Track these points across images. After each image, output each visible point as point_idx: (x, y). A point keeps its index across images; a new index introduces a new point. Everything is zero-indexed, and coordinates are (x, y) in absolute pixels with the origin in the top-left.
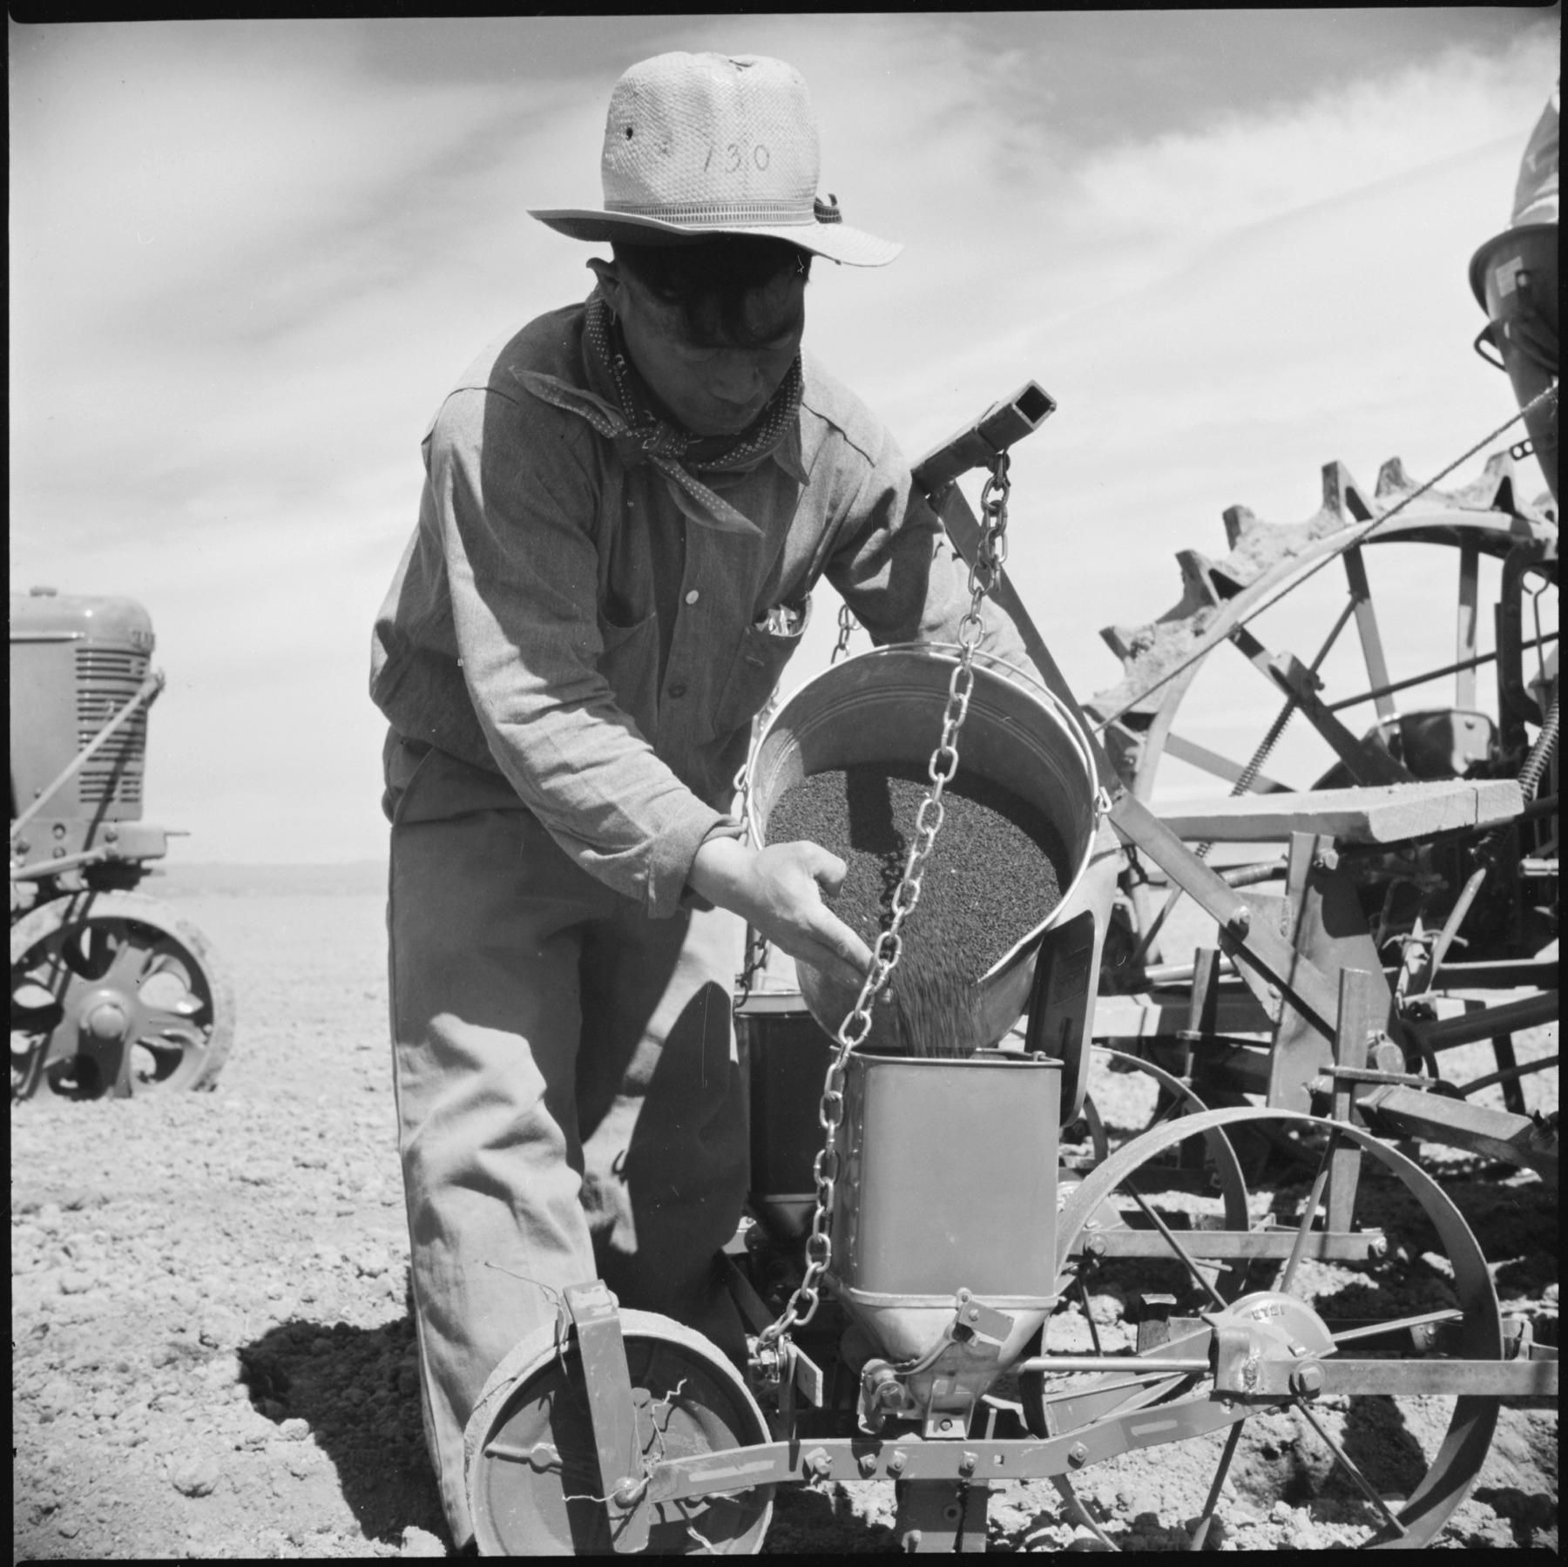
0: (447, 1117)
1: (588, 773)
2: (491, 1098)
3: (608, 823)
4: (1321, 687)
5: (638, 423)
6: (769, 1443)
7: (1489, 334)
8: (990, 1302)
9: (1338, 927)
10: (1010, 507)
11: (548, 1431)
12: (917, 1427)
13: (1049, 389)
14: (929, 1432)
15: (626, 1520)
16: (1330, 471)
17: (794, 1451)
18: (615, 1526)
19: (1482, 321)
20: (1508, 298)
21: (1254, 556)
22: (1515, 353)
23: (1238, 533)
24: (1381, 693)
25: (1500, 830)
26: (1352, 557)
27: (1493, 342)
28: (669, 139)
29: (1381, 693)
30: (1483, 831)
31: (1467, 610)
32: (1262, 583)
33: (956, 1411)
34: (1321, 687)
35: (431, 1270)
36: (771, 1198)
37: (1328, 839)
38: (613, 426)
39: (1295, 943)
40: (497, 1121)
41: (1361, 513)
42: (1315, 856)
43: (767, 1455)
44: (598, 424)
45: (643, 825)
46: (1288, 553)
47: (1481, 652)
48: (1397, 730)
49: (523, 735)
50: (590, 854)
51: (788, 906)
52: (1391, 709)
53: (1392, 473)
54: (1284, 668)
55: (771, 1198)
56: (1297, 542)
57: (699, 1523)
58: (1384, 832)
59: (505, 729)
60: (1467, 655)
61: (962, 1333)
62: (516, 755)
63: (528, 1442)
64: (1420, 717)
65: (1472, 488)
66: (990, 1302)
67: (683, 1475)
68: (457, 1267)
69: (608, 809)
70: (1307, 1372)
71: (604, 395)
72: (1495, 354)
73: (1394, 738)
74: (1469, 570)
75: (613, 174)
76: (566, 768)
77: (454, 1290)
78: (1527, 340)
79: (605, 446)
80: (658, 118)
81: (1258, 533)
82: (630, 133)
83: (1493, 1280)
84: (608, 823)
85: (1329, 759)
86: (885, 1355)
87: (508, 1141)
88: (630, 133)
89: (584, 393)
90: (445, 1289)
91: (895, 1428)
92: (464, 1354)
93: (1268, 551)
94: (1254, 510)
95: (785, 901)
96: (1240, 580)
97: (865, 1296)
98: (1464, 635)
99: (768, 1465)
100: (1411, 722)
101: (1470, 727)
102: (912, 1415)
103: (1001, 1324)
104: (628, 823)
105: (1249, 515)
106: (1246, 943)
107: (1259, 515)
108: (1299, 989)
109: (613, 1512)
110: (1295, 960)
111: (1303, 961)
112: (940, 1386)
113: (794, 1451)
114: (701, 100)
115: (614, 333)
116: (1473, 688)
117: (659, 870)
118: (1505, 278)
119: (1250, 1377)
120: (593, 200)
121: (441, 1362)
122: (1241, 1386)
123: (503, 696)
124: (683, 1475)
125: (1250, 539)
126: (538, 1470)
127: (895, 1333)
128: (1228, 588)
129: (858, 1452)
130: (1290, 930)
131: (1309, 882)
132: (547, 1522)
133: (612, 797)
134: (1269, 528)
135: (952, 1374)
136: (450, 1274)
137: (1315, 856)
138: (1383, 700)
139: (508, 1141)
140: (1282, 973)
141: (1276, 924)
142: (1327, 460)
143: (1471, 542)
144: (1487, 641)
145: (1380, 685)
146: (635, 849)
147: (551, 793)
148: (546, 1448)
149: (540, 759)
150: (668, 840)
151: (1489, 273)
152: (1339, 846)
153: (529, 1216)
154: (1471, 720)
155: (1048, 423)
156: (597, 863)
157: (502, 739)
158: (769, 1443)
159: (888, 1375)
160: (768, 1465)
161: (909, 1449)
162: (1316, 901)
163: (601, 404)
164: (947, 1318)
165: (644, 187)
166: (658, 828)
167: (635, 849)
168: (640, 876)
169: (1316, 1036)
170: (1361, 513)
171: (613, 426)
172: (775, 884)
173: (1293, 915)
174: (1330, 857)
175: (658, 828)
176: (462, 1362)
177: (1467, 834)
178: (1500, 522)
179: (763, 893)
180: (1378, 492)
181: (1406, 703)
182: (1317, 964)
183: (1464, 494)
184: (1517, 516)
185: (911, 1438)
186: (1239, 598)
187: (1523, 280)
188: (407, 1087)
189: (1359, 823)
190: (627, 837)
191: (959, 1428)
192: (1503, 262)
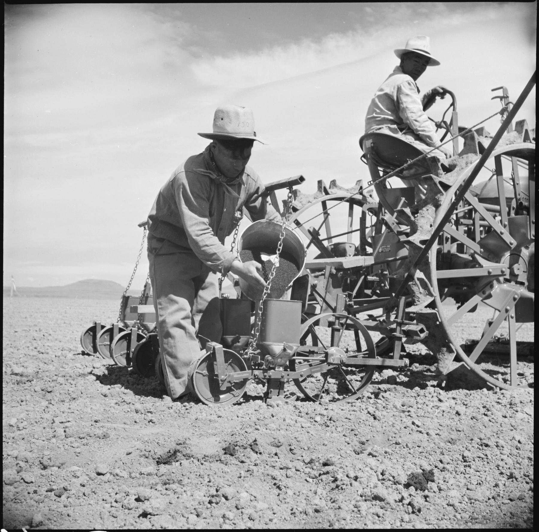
0: (172, 314)
1: (211, 247)
2: (182, 309)
3: (214, 257)
4: (320, 235)
5: (218, 176)
6: (247, 371)
7: (364, 156)
8: (291, 344)
9: (334, 287)
10: (468, 245)
11: (206, 369)
12: (274, 369)
13: (304, 177)
14: (276, 369)
15: (223, 384)
16: (320, 182)
17: (252, 372)
18: (220, 385)
19: (362, 153)
20: (369, 148)
21: (301, 202)
22: (370, 161)
23: (297, 196)
24: (329, 238)
25: (368, 267)
26: (324, 203)
27: (365, 158)
28: (231, 120)
29: (329, 238)
30: (364, 267)
31: (350, 218)
32: (303, 209)
33: (281, 366)
34: (320, 235)
35: (168, 344)
36: (225, 337)
37: (333, 268)
38: (214, 176)
39: (326, 289)
40: (183, 314)
41: (327, 193)
42: (331, 271)
43: (247, 373)
44: (211, 176)
45: (222, 257)
46: (309, 202)
47: (354, 229)
48: (333, 247)
49: (198, 239)
50: (210, 263)
51: (251, 273)
52: (331, 242)
53: (333, 183)
54: (311, 230)
55: (225, 337)
56: (311, 199)
57: (233, 386)
58: (346, 266)
59: (194, 237)
60: (350, 230)
61: (285, 350)
62: (196, 243)
63: (203, 370)
64: (339, 244)
65: (353, 188)
66: (291, 344)
67: (233, 376)
68: (174, 343)
69: (215, 254)
70: (344, 359)
71: (212, 171)
72: (365, 161)
73: (332, 249)
74: (351, 208)
75: (215, 125)
76: (207, 246)
77: (174, 348)
78: (373, 159)
79: (211, 180)
80: (228, 116)
81: (301, 196)
82: (222, 119)
83: (375, 346)
84: (214, 257)
85: (318, 252)
86: (269, 354)
87: (185, 318)
88: (222, 119)
89: (209, 171)
90: (171, 347)
91: (270, 369)
92: (176, 360)
93: (304, 201)
94: (301, 190)
95: (251, 273)
96: (298, 208)
97: (267, 343)
98: (350, 224)
99: (248, 374)
100: (337, 245)
101: (350, 247)
102: (273, 366)
103: (291, 348)
104: (219, 257)
105: (300, 191)
106: (316, 289)
107: (302, 192)
108: (327, 299)
109: (220, 382)
110: (326, 293)
111: (328, 294)
112: (279, 360)
113: (252, 372)
114: (237, 114)
115: (213, 159)
116: (351, 237)
117: (224, 266)
118: (368, 143)
119: (333, 361)
120: (211, 131)
121: (170, 363)
122: (332, 362)
123: (194, 231)
124: (233, 376)
125: (300, 198)
126: (204, 376)
127: (272, 350)
128: (295, 210)
129: (263, 373)
130: (325, 287)
131: (329, 276)
132: (205, 386)
133: (216, 252)
134: (304, 195)
135: (281, 358)
136: (173, 344)
137: (331, 271)
138: (330, 240)
139: (185, 318)
140: (323, 296)
141: (322, 285)
142: (319, 179)
143: (352, 202)
144: (357, 225)
145: (329, 236)
146: (220, 262)
147: (203, 251)
148: (205, 372)
149: (201, 244)
150: (226, 260)
151: (364, 142)
152: (335, 269)
153: (189, 333)
154: (351, 245)
155: (304, 183)
156: (212, 265)
157: (194, 240)
158: (247, 371)
159: (270, 358)
160: (248, 374)
161: (272, 373)
162: (331, 280)
163: (211, 172)
164: (282, 347)
165: (225, 129)
166: (224, 258)
167: (220, 262)
168: (220, 267)
169: (329, 309)
170: (327, 193)
171: (214, 176)
172: (248, 269)
173: (326, 284)
174: (334, 271)
175: (224, 258)
176: (175, 362)
177: (361, 268)
178: (360, 197)
179: (245, 271)
180: (330, 188)
181: (335, 241)
182: (330, 294)
183: (351, 190)
184: (364, 196)
185: (272, 371)
186: (298, 212)
187: (372, 145)
188: (160, 308)
189: (341, 264)
190: (218, 259)
191: (281, 369)
192: (367, 140)
